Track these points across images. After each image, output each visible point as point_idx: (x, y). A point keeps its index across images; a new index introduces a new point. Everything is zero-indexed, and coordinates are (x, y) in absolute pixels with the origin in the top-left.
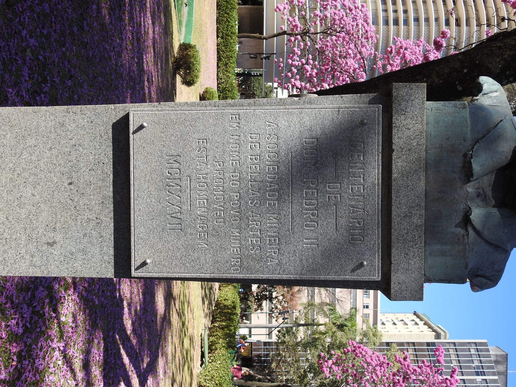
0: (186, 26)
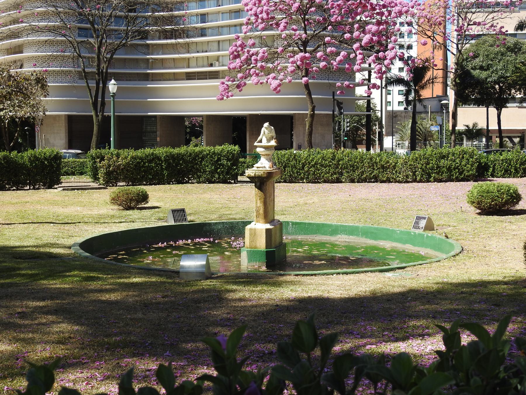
0: (375, 239)
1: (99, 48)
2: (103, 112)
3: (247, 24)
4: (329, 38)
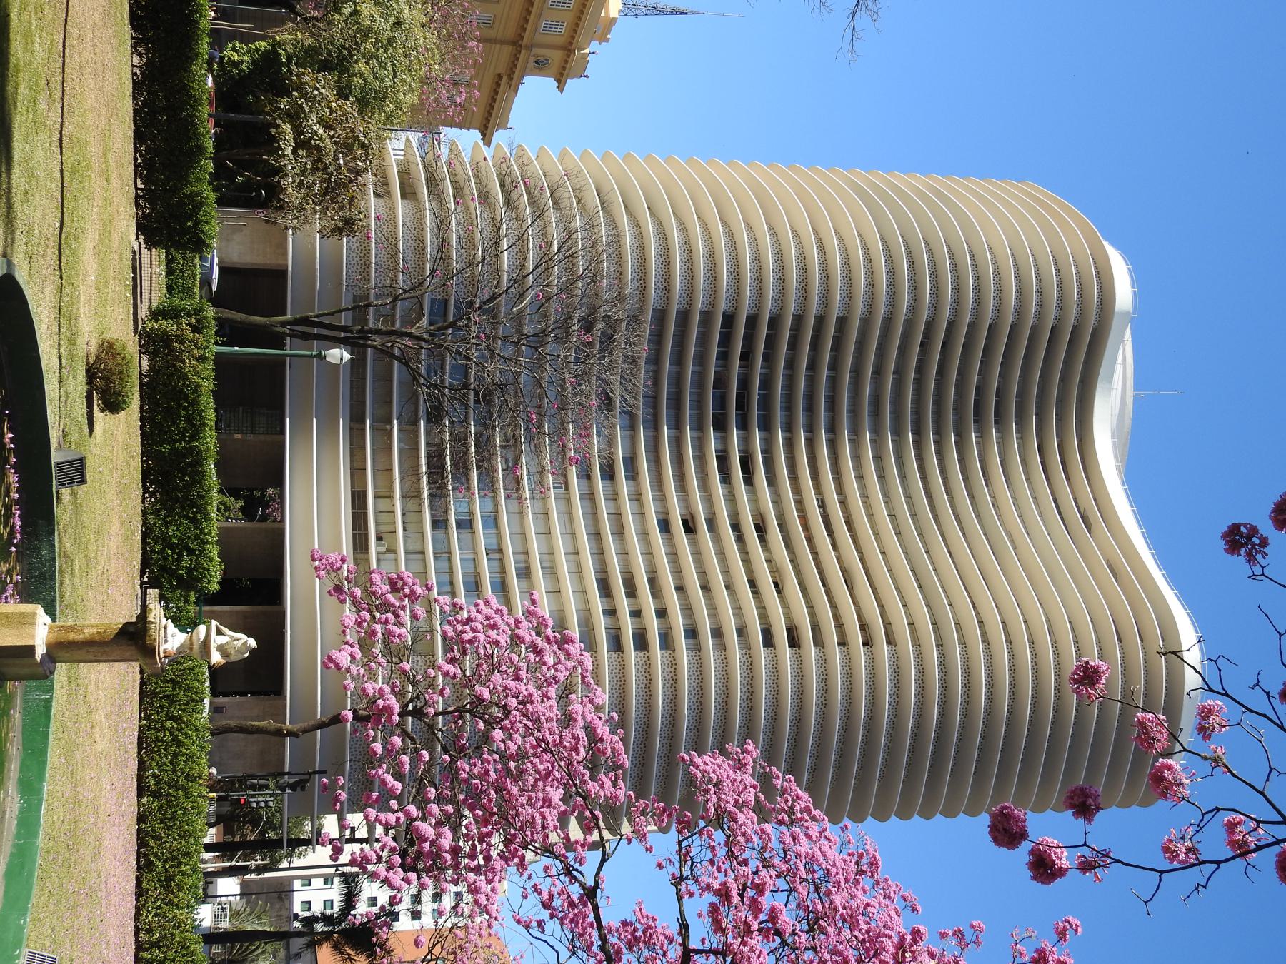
1: (410, 335)
2: (291, 336)
3: (454, 605)
4: (427, 759)
